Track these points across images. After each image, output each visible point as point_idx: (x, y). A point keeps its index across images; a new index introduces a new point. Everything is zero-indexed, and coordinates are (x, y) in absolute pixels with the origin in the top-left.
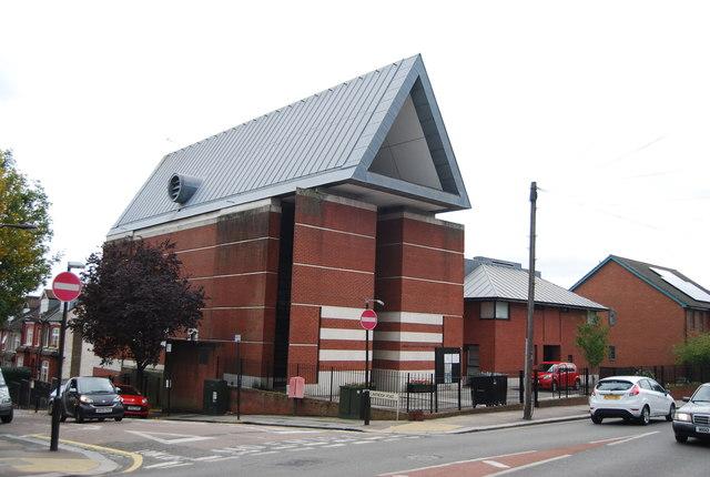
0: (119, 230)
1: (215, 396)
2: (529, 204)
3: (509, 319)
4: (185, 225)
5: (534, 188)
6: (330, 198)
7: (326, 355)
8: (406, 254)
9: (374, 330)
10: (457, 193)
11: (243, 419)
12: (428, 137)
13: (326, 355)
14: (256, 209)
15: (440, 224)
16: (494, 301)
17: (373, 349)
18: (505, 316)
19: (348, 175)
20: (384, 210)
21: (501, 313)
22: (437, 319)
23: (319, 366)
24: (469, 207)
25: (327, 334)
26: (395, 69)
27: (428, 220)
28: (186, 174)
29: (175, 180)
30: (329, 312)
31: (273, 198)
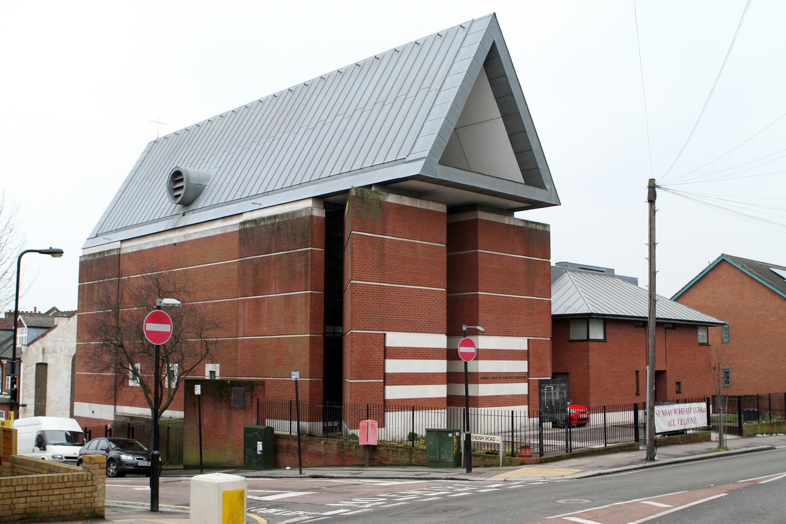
0: (100, 240)
1: (260, 446)
2: (647, 205)
3: (605, 340)
4: (194, 234)
5: (652, 187)
6: (392, 199)
7: (393, 392)
8: (481, 264)
9: (22, 352)
10: (543, 187)
11: (307, 472)
12: (505, 117)
13: (393, 392)
14: (293, 213)
15: (521, 224)
16: (586, 319)
17: (310, 381)
18: (601, 336)
19: (415, 169)
20: (453, 209)
21: (597, 333)
22: (520, 343)
23: (387, 406)
24: (558, 203)
25: (393, 366)
26: (461, 34)
27: (507, 220)
28: (192, 170)
29: (177, 176)
30: (394, 339)
31: (316, 198)
